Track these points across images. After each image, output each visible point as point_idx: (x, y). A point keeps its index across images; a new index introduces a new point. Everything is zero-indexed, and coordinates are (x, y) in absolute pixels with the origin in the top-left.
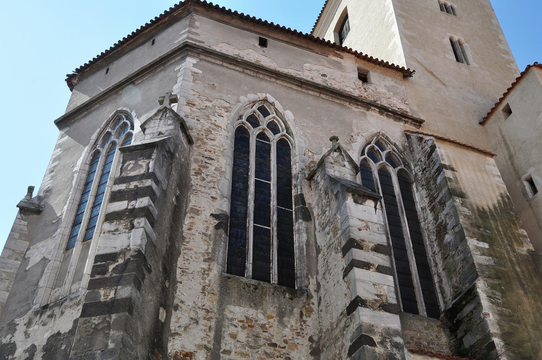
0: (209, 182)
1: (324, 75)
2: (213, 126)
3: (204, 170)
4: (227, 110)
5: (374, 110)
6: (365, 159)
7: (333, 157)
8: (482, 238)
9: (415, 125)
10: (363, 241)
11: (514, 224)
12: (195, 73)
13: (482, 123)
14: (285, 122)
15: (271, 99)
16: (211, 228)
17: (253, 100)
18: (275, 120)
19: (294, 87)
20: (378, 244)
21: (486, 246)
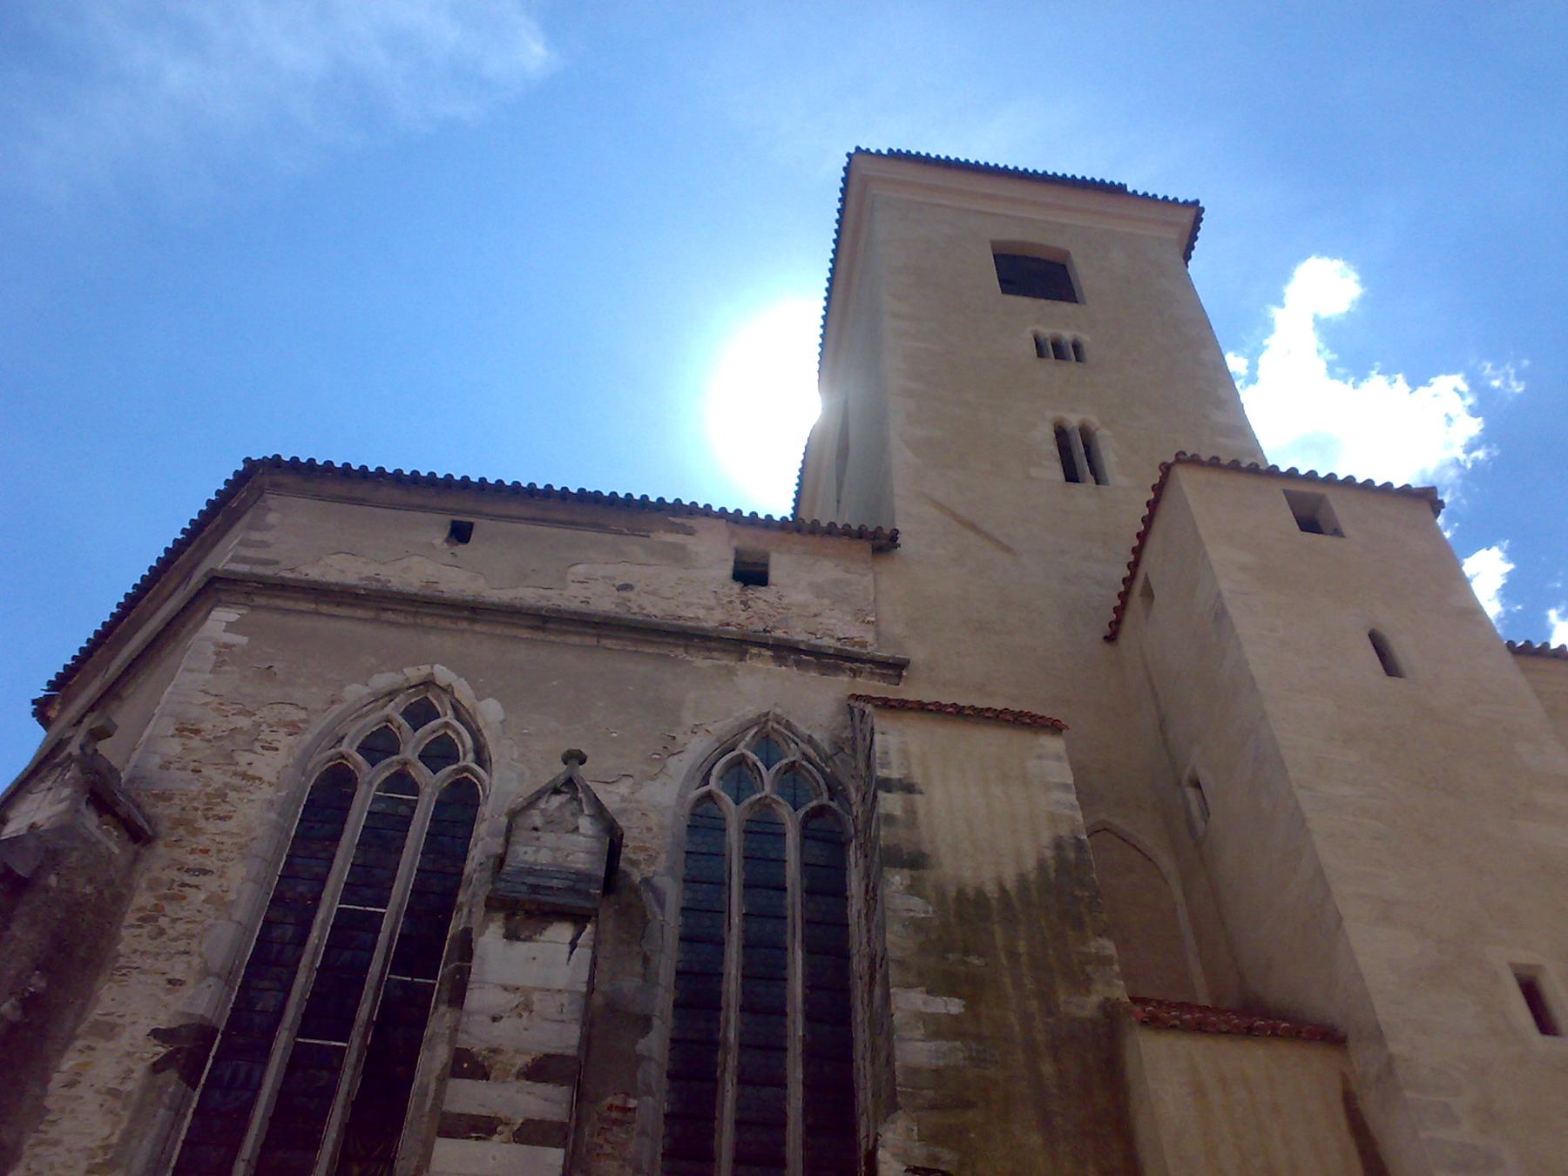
0: (175, 940)
1: (626, 587)
2: (237, 781)
3: (170, 909)
4: (294, 728)
5: (759, 655)
6: (709, 796)
7: (543, 811)
8: (945, 984)
9: (884, 677)
10: (495, 1051)
11: (1079, 924)
12: (226, 646)
13: (1111, 638)
14: (476, 734)
15: (443, 674)
16: (140, 1070)
17: (389, 688)
18: (450, 733)
19: (525, 634)
20: (548, 1056)
21: (955, 1006)
